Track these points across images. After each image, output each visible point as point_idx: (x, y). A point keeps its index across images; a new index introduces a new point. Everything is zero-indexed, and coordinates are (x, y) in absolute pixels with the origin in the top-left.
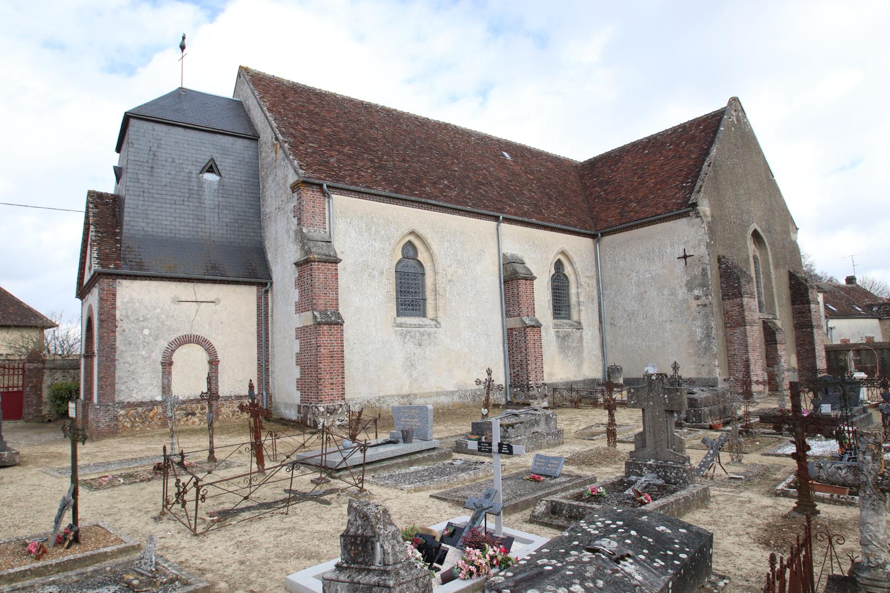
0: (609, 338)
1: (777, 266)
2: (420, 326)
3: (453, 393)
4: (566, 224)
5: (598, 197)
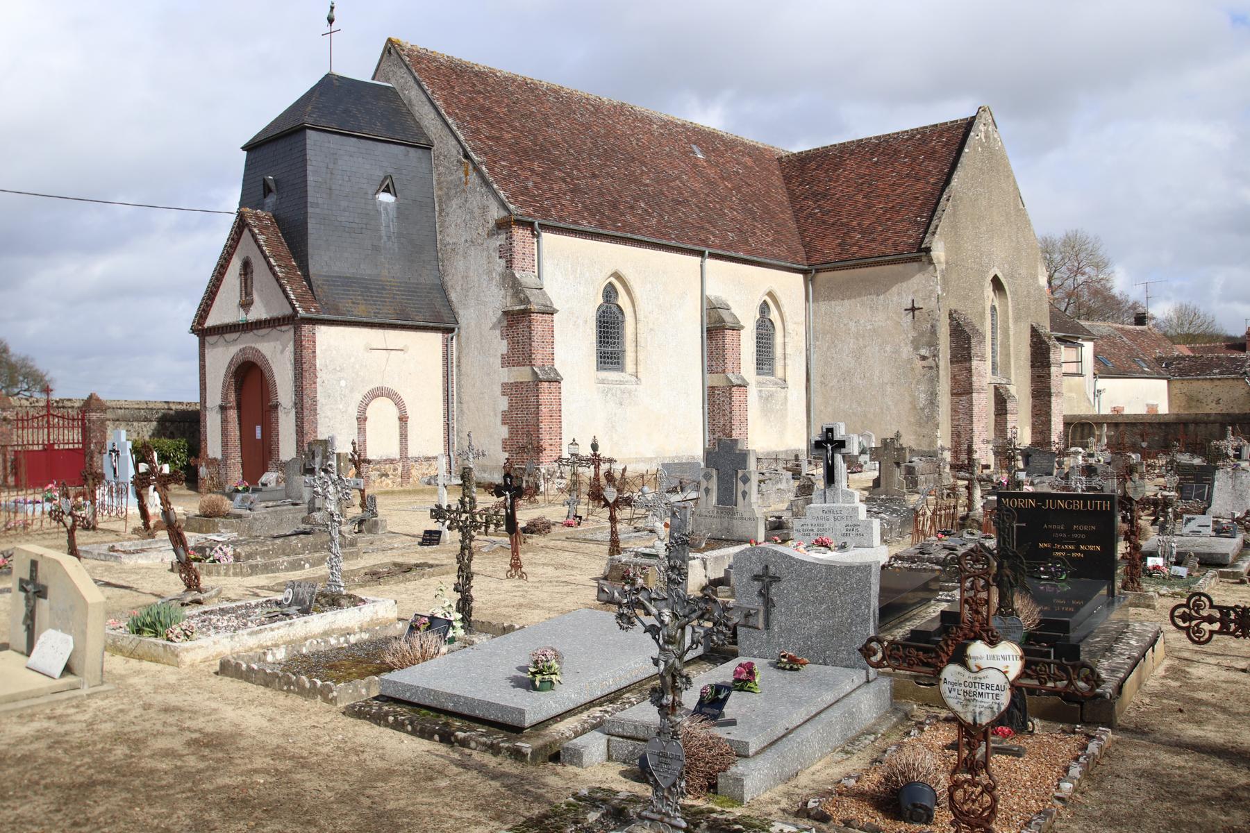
0: (817, 400)
1: (1017, 319)
2: (621, 383)
3: (651, 459)
4: (768, 256)
5: (811, 215)
